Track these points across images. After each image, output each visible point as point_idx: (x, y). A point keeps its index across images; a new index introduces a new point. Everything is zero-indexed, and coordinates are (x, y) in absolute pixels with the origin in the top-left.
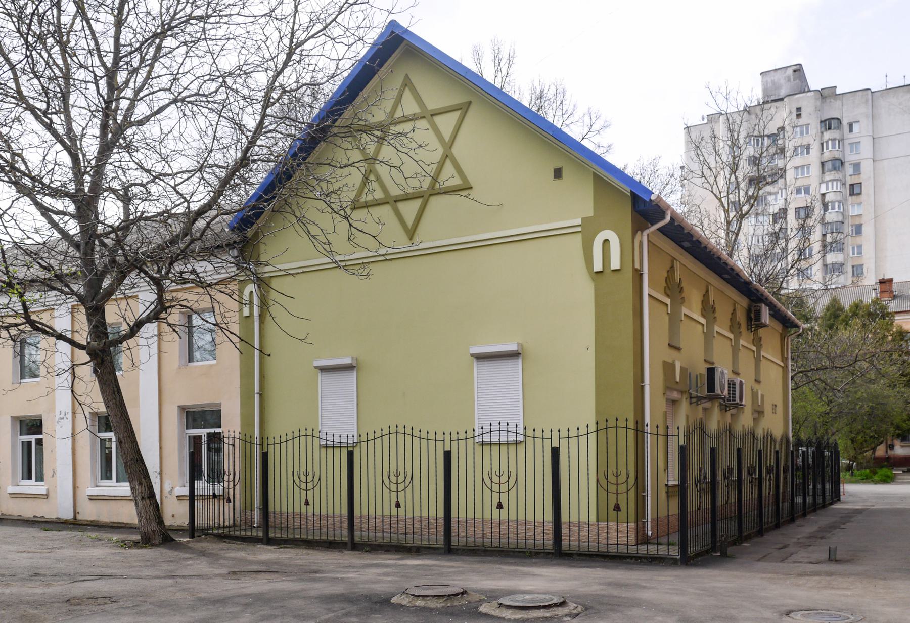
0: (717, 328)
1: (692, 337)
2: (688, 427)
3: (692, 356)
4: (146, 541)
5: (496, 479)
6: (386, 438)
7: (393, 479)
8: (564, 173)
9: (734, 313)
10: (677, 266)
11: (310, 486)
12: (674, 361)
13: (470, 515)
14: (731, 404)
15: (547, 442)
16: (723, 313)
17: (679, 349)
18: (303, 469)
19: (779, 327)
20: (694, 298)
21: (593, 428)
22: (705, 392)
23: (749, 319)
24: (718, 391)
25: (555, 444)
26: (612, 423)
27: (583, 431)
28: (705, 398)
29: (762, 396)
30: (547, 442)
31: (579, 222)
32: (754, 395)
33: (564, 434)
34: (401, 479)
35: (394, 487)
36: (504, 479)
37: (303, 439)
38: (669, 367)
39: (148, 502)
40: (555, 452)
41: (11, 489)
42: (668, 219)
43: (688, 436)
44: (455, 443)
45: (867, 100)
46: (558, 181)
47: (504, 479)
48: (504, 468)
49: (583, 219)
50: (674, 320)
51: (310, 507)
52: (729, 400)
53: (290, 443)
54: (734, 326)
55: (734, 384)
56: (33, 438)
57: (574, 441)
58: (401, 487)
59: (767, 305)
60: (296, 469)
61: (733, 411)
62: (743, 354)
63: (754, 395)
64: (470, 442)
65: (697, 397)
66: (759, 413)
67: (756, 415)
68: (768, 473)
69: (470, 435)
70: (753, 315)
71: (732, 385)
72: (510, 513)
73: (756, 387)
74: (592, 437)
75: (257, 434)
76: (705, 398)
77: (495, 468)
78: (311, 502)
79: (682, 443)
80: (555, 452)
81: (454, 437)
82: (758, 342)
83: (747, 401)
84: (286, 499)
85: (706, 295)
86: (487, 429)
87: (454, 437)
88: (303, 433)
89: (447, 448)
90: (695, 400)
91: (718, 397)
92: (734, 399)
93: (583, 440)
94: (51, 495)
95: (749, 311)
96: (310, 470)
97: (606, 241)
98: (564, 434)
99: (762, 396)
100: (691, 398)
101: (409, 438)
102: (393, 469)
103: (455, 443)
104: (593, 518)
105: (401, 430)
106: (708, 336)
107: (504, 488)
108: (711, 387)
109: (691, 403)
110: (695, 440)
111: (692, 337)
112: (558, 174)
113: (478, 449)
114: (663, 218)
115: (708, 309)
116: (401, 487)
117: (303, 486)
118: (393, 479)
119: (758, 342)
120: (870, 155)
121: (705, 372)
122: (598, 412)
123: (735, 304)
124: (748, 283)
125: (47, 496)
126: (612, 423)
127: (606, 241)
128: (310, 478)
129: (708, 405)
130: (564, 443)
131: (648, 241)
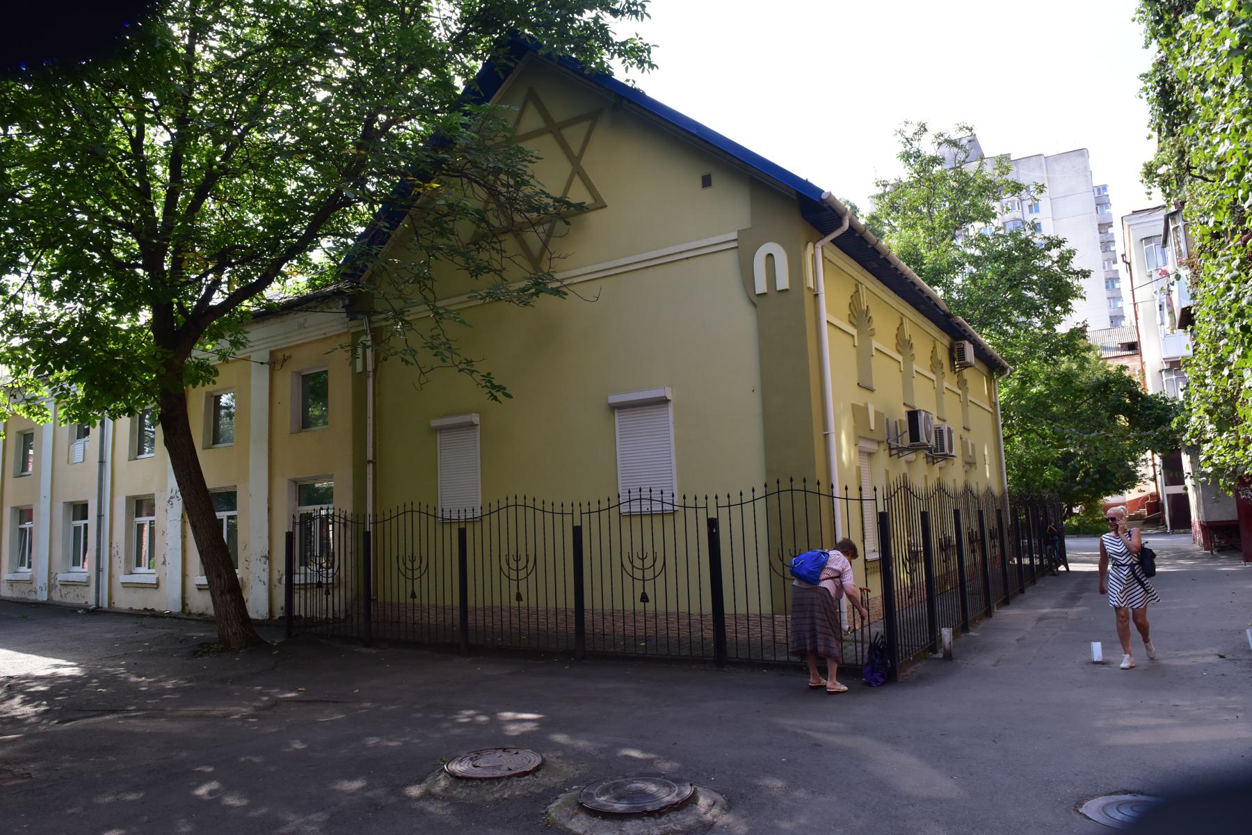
0: (915, 367)
1: (886, 374)
2: (888, 487)
3: (890, 401)
4: (223, 646)
5: (638, 563)
6: (503, 512)
7: (513, 564)
8: (714, 181)
9: (934, 351)
10: (863, 291)
11: (417, 574)
12: (866, 404)
13: (618, 606)
14: (938, 453)
15: (702, 513)
16: (922, 349)
17: (872, 390)
18: (409, 553)
19: (984, 369)
20: (883, 340)
21: (760, 492)
22: (906, 441)
23: (952, 359)
24: (923, 439)
25: (713, 515)
26: (785, 485)
27: (748, 496)
28: (907, 449)
29: (973, 446)
30: (702, 513)
31: (734, 236)
32: (964, 444)
33: (723, 501)
34: (522, 564)
35: (513, 575)
36: (648, 562)
37: (409, 515)
38: (859, 413)
39: (228, 597)
40: (713, 524)
41: (124, 578)
42: (846, 225)
43: (889, 498)
44: (585, 517)
45: (1041, 165)
46: (708, 190)
47: (648, 562)
48: (648, 548)
49: (739, 232)
50: (864, 358)
51: (417, 601)
52: (936, 450)
53: (394, 520)
54: (935, 365)
55: (941, 432)
56: (81, 523)
57: (736, 511)
58: (522, 574)
59: (971, 342)
60: (401, 553)
61: (942, 463)
62: (948, 397)
63: (964, 444)
64: (614, 511)
65: (898, 448)
66: (970, 464)
67: (967, 467)
68: (992, 537)
69: (614, 502)
70: (956, 356)
71: (939, 433)
72: (658, 604)
73: (965, 434)
74: (761, 504)
75: (370, 510)
76: (907, 449)
77: (637, 548)
78: (418, 594)
79: (881, 509)
80: (713, 524)
81: (585, 509)
82: (962, 383)
83: (957, 451)
84: (393, 588)
85: (900, 328)
86: (635, 495)
87: (585, 509)
88: (409, 508)
89: (577, 523)
90: (896, 451)
91: (924, 447)
92: (943, 450)
93: (748, 508)
94: (162, 585)
95: (951, 351)
96: (417, 554)
97: (770, 256)
98: (723, 501)
99: (973, 446)
100: (890, 449)
101: (424, 517)
102: (512, 552)
103: (585, 517)
104: (767, 609)
105: (521, 501)
106: (908, 377)
107: (649, 574)
108: (914, 435)
109: (891, 456)
110: (899, 501)
111: (886, 374)
112: (706, 182)
113: (626, 522)
114: (840, 224)
115: (904, 345)
116: (522, 574)
117: (409, 574)
118: (513, 564)
119: (962, 383)
120: (1050, 215)
121: (905, 418)
122: (769, 471)
123: (935, 339)
124: (948, 316)
125: (156, 586)
126: (785, 485)
127: (770, 256)
128: (417, 564)
129: (912, 456)
130: (724, 513)
131: (824, 257)
